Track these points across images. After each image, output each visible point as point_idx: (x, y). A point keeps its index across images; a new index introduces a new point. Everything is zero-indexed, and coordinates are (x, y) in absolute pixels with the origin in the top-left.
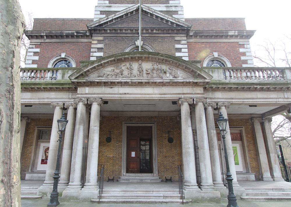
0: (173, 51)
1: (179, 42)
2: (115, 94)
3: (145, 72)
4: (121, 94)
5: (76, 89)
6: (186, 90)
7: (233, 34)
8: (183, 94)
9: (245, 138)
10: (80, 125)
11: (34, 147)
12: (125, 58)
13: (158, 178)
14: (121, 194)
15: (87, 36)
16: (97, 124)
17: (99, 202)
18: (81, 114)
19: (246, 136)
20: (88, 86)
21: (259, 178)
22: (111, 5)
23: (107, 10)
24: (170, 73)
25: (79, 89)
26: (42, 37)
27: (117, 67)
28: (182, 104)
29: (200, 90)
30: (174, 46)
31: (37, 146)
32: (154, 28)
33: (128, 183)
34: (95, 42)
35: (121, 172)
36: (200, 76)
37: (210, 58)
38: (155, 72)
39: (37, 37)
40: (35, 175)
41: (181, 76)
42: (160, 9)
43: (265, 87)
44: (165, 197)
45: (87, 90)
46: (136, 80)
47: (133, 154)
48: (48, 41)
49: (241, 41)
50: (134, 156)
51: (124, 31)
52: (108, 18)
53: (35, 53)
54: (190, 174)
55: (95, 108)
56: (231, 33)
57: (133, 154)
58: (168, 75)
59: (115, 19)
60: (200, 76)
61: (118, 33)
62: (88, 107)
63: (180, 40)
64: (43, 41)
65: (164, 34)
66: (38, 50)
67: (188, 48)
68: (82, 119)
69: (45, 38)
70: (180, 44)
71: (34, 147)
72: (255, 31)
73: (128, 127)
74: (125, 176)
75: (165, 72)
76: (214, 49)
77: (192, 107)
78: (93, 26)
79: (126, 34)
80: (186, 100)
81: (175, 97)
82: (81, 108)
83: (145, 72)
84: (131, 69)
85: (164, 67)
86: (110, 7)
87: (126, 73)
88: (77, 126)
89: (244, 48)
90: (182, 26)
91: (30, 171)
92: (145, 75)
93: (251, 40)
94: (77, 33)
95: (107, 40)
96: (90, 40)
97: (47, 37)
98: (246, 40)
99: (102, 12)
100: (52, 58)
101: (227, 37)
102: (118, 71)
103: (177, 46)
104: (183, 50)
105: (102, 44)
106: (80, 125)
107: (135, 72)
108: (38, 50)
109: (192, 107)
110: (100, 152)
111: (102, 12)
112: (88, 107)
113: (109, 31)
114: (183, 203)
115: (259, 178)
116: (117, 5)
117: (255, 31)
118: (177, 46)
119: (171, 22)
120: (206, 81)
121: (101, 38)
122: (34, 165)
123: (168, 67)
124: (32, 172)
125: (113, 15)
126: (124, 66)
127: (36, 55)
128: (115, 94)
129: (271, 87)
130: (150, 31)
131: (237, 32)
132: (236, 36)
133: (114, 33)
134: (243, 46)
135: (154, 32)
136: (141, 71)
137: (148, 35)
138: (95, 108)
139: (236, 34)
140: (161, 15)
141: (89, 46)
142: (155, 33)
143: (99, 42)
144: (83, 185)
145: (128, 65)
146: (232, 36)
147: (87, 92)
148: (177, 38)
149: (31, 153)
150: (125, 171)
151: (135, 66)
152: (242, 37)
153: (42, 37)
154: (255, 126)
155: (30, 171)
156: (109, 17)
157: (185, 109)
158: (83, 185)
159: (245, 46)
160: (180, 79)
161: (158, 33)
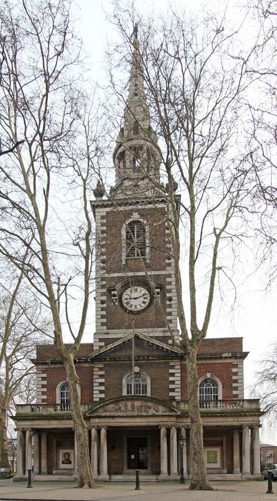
0: (167, 376)
1: (173, 367)
2: (116, 423)
3: (136, 408)
4: (120, 423)
5: (90, 420)
6: (164, 419)
7: (227, 356)
8: (162, 422)
9: (224, 445)
10: (94, 441)
11: (55, 453)
12: (122, 400)
13: (150, 471)
14: (122, 478)
15: (88, 362)
16: (106, 441)
17: (110, 482)
18: (95, 435)
19: (226, 443)
20: (97, 418)
21: (231, 471)
22: (109, 331)
23: (105, 337)
24: (154, 409)
25: (91, 420)
26: (47, 363)
27: (116, 405)
28: (161, 428)
29: (173, 419)
30: (168, 371)
31: (58, 453)
32: (150, 356)
33: (128, 474)
34: (97, 369)
35: (123, 468)
36: (173, 411)
37: (203, 379)
38: (143, 408)
39: (42, 364)
40: (60, 471)
41: (161, 410)
42: (157, 334)
43: (223, 415)
44: (147, 479)
45: (97, 420)
46: (129, 414)
47: (133, 457)
48: (52, 366)
49: (234, 361)
50: (104, 395)
51: (122, 359)
52: (107, 348)
53: (43, 379)
54: (164, 467)
55: (103, 431)
56: (224, 355)
57: (133, 457)
58: (152, 410)
59: (113, 348)
60: (173, 411)
61: (116, 361)
62: (99, 431)
63: (174, 366)
64: (48, 367)
65: (159, 360)
66: (45, 375)
67: (181, 373)
68: (95, 438)
69: (50, 364)
70: (174, 369)
71: (55, 453)
72: (249, 352)
73: (128, 439)
74: (126, 470)
75: (150, 408)
76: (208, 370)
77: (168, 430)
78: (94, 356)
79: (124, 361)
80: (164, 425)
81: (157, 424)
82: (94, 432)
83: (136, 408)
84: (126, 406)
85: (150, 404)
86: (108, 334)
87: (123, 408)
88: (93, 443)
89: (237, 368)
90: (176, 353)
91: (55, 468)
92: (136, 410)
93: (246, 361)
94: (79, 359)
95: (107, 367)
96: (92, 365)
97: (52, 363)
98: (240, 360)
99: (101, 340)
100: (59, 381)
101: (221, 358)
102: (117, 408)
103: (171, 371)
104: (176, 375)
105: (103, 371)
106: (94, 441)
107: (129, 408)
108: (45, 375)
109: (168, 430)
110: (108, 455)
111: (101, 340)
112: (99, 431)
113: (108, 359)
114: (156, 482)
115: (231, 471)
116: (115, 330)
117: (249, 352)
118: (171, 371)
119: (166, 349)
120: (178, 414)
121: (102, 366)
122: (57, 465)
123: (152, 404)
124: (57, 469)
125: (112, 345)
126: (121, 405)
127: (44, 380)
128: (116, 423)
129: (228, 415)
130: (146, 358)
131: (230, 354)
132: (231, 358)
133: (113, 361)
134: (236, 366)
135: (150, 358)
136: (133, 407)
137: (144, 362)
138: (103, 431)
139: (230, 356)
140: (157, 343)
141: (91, 371)
142: (151, 360)
143: (101, 369)
144: (99, 474)
145: (124, 403)
146: (226, 358)
147: (97, 421)
148: (171, 364)
149: (53, 456)
150: (126, 467)
151: (129, 404)
152: (236, 358)
153: (47, 363)
154: (234, 436)
155: (55, 468)
156: (108, 346)
157: (163, 431)
158: (99, 474)
159: (239, 365)
160: (160, 413)
161: (154, 360)
